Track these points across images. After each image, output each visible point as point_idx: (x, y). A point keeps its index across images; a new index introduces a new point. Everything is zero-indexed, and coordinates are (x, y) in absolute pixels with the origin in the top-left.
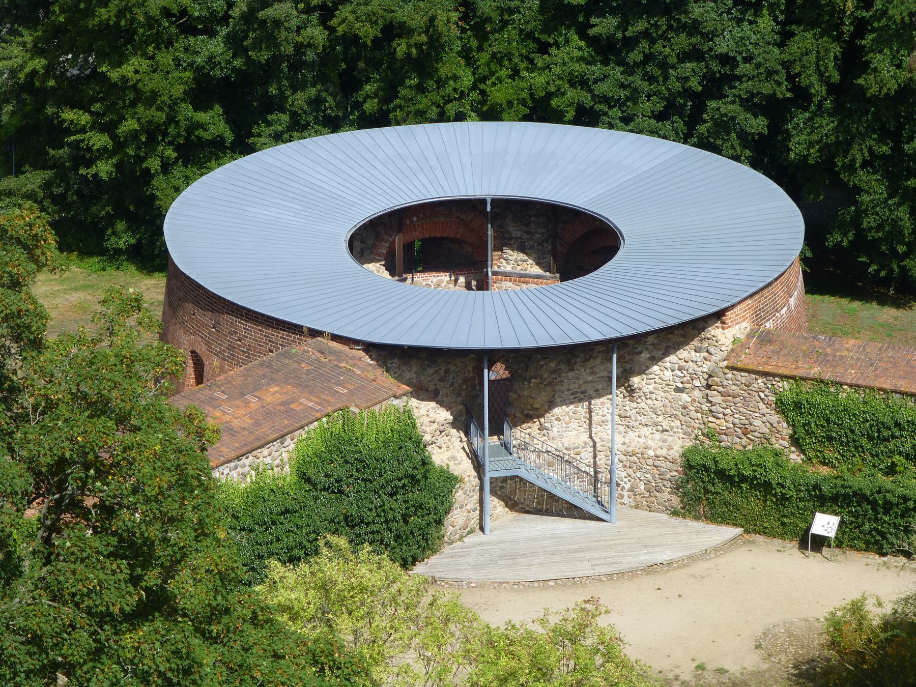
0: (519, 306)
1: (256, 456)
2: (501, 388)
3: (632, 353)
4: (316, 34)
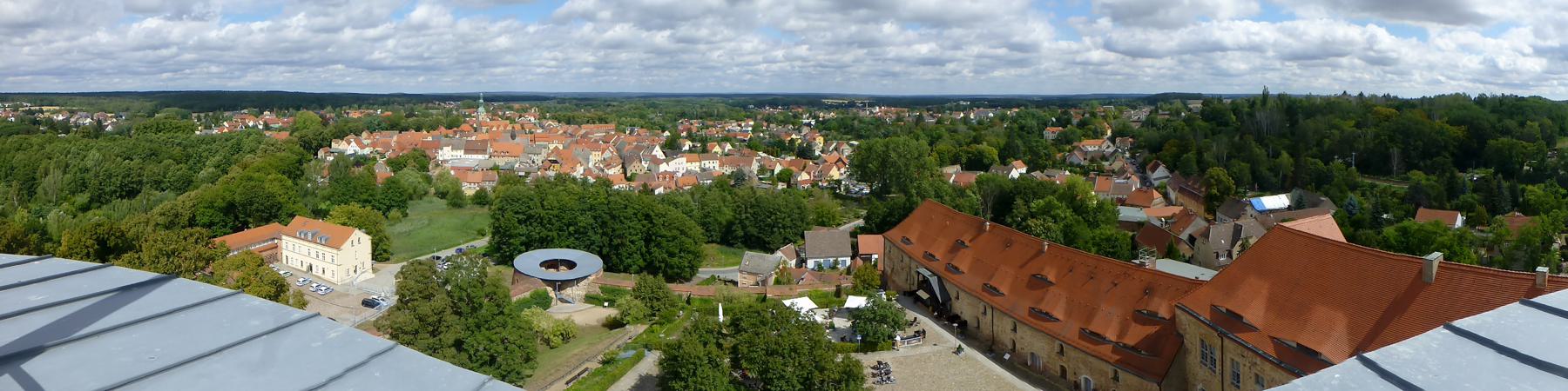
0: (563, 274)
1: (519, 294)
2: (560, 285)
3: (578, 280)
4: (842, 323)
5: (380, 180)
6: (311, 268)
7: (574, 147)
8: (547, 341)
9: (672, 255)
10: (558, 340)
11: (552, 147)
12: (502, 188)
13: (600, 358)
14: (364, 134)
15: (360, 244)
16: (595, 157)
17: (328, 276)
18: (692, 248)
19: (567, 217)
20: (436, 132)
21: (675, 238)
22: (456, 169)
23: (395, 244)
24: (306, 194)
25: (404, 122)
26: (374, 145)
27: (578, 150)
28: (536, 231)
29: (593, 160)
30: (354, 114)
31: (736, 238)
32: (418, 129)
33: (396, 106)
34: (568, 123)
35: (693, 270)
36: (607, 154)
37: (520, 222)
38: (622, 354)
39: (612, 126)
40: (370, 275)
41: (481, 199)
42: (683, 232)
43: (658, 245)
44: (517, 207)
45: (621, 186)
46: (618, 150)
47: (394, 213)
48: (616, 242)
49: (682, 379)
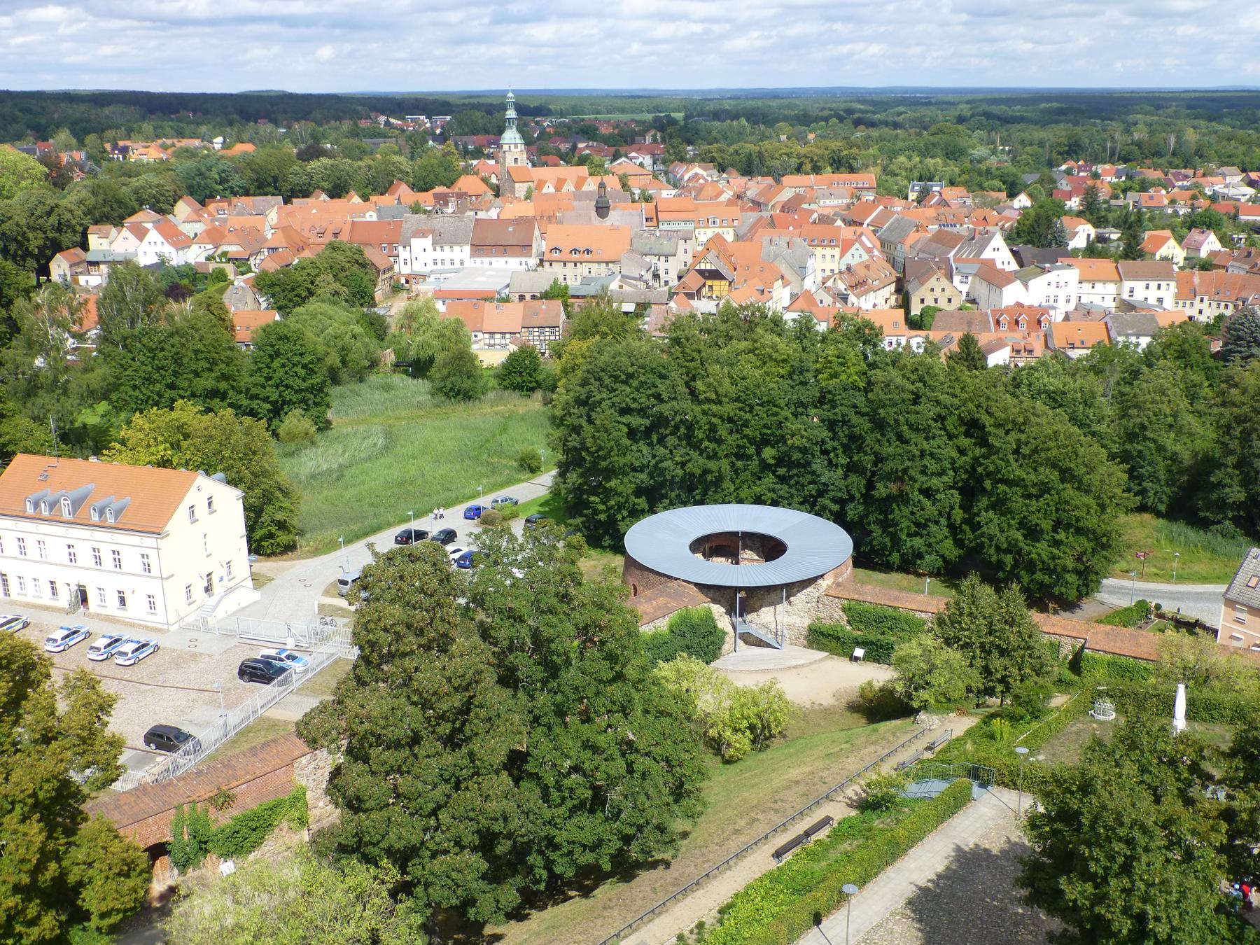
0: (750, 571)
2: (742, 601)
3: (791, 589)
5: (242, 334)
6: (83, 597)
7: (764, 235)
8: (716, 745)
9: (1033, 533)
10: (742, 742)
11: (705, 235)
12: (576, 345)
13: (854, 791)
14: (183, 208)
15: (212, 512)
16: (823, 264)
17: (136, 610)
18: (1091, 522)
19: (757, 423)
20: (387, 200)
21: (1044, 489)
22: (456, 297)
23: (309, 505)
24: (32, 388)
25: (297, 172)
26: (215, 236)
27: (775, 244)
28: (675, 459)
29: (815, 268)
30: (146, 153)
31: (1221, 505)
32: (337, 191)
33: (265, 128)
34: (748, 170)
35: (1088, 580)
36: (856, 256)
37: (632, 433)
38: (913, 789)
39: (869, 177)
40: (248, 595)
41: (521, 375)
42: (1067, 475)
43: (999, 505)
44: (625, 394)
45: (897, 338)
46: (885, 244)
47: (295, 421)
48: (882, 490)
49: (1087, 876)
